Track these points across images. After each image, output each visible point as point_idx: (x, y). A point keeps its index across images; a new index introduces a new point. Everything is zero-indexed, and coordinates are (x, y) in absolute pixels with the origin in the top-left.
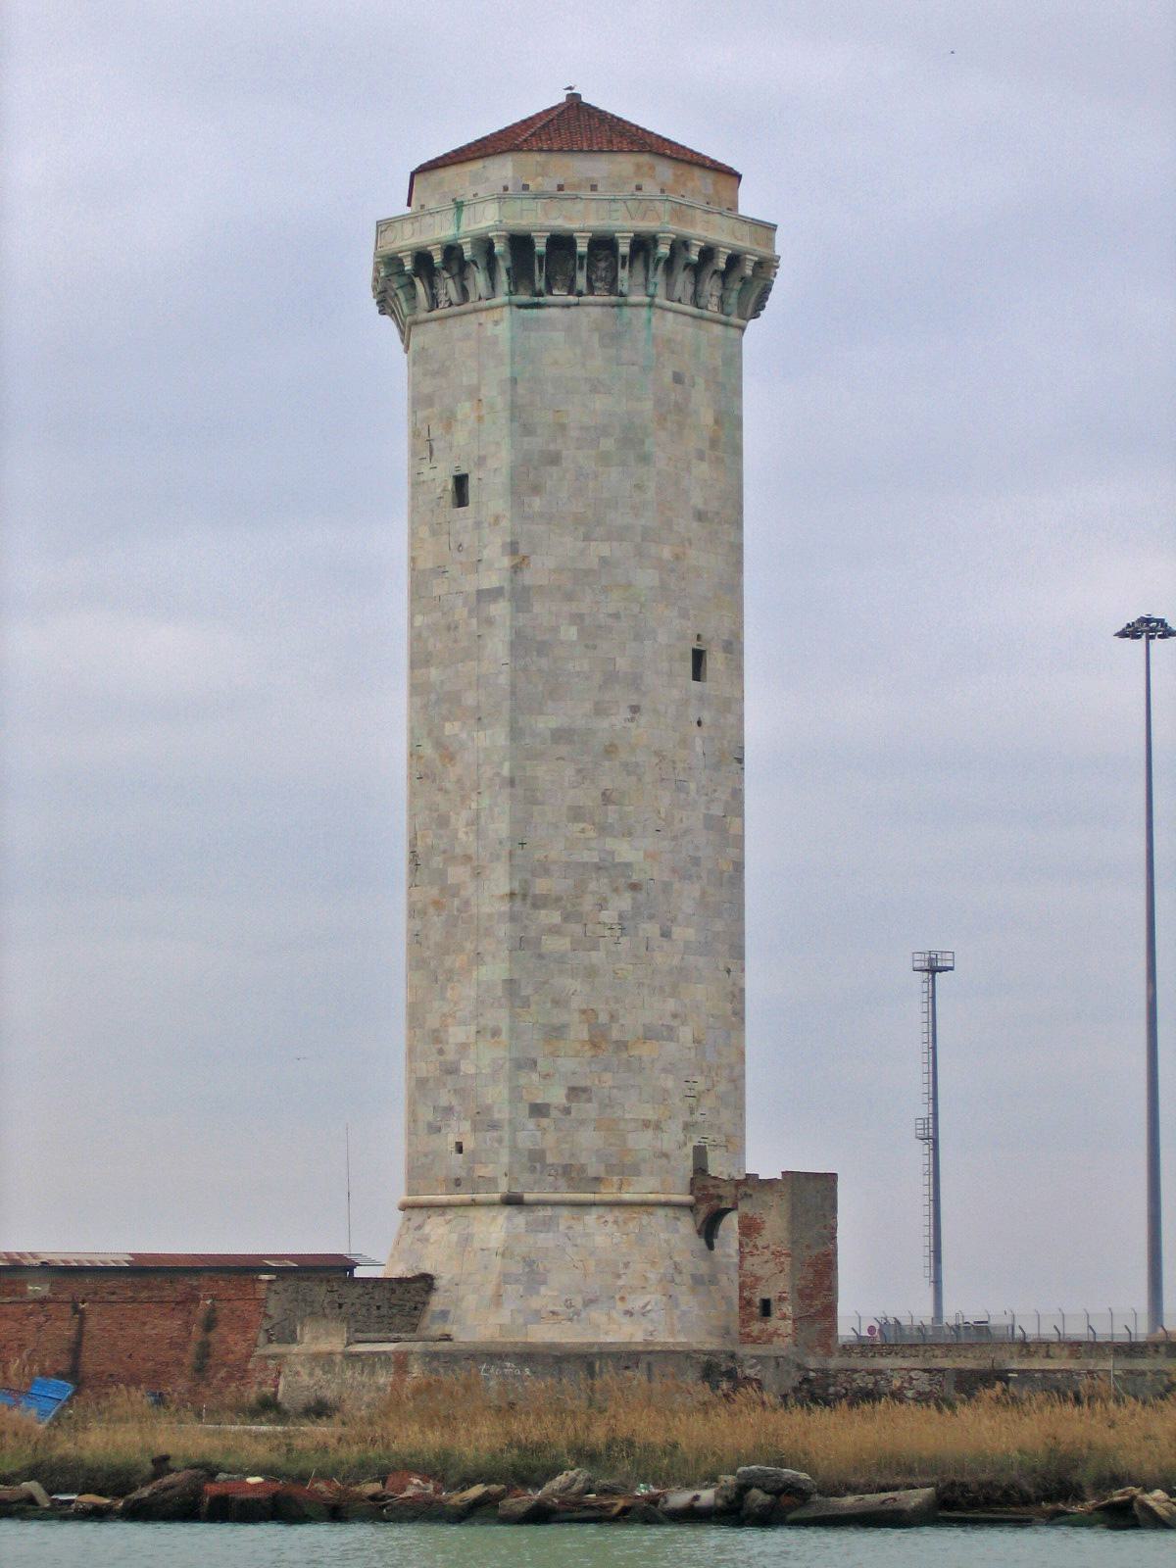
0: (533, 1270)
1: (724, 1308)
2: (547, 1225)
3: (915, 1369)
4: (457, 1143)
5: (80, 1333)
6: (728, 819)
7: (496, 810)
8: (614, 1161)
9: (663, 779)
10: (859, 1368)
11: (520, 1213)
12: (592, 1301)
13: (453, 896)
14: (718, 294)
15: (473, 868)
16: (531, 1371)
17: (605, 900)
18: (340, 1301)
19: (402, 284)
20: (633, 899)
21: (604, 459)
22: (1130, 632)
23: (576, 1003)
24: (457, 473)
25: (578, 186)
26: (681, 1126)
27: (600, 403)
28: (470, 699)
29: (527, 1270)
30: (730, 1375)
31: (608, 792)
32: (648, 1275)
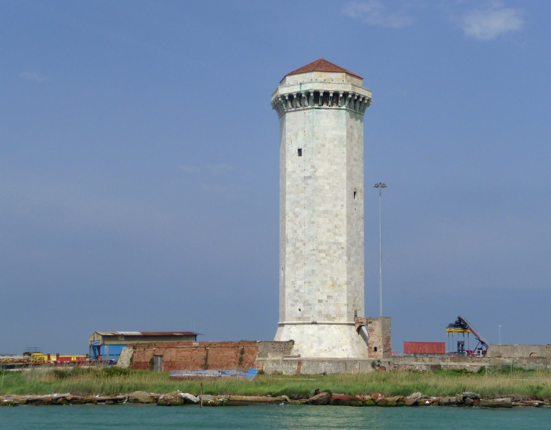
2: (323, 329)
14: (359, 107)
16: (332, 365)
17: (336, 251)
20: (342, 251)
23: (329, 276)
24: (299, 148)
28: (302, 202)
30: (379, 366)
32: (347, 341)
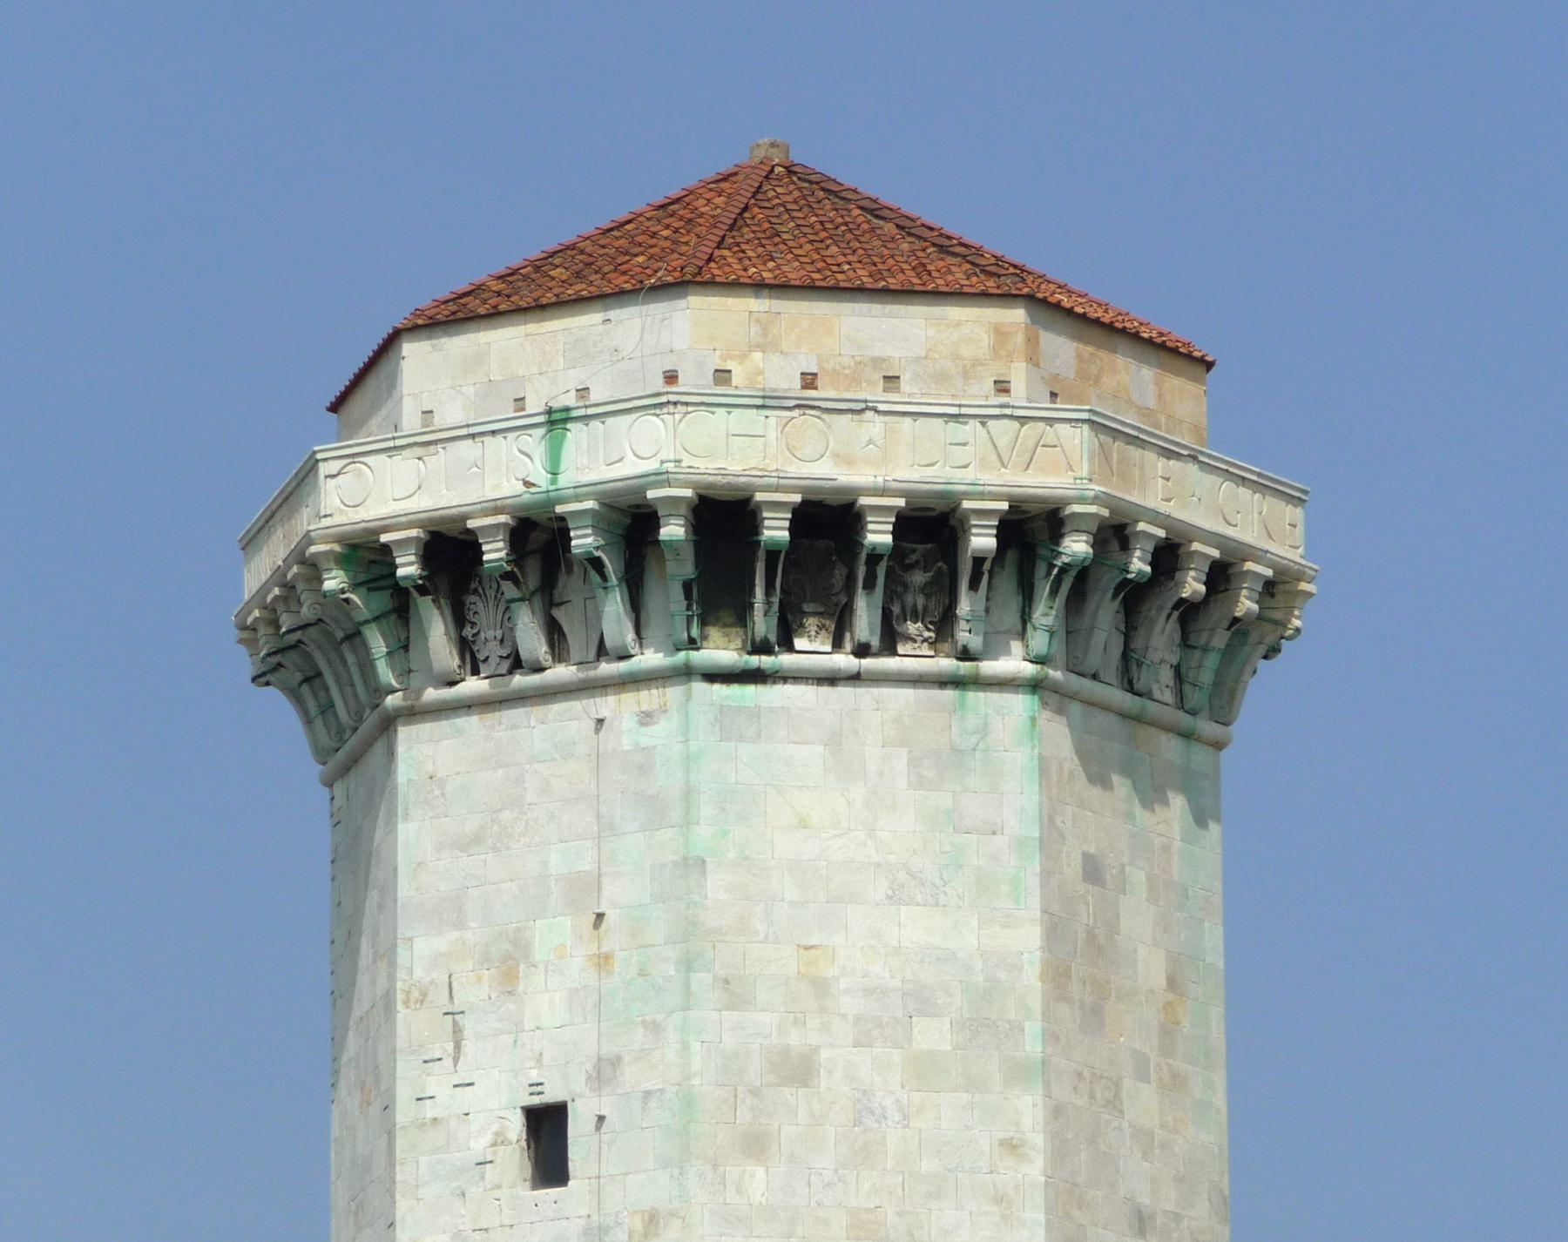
21: (924, 1071)
24: (536, 1101)
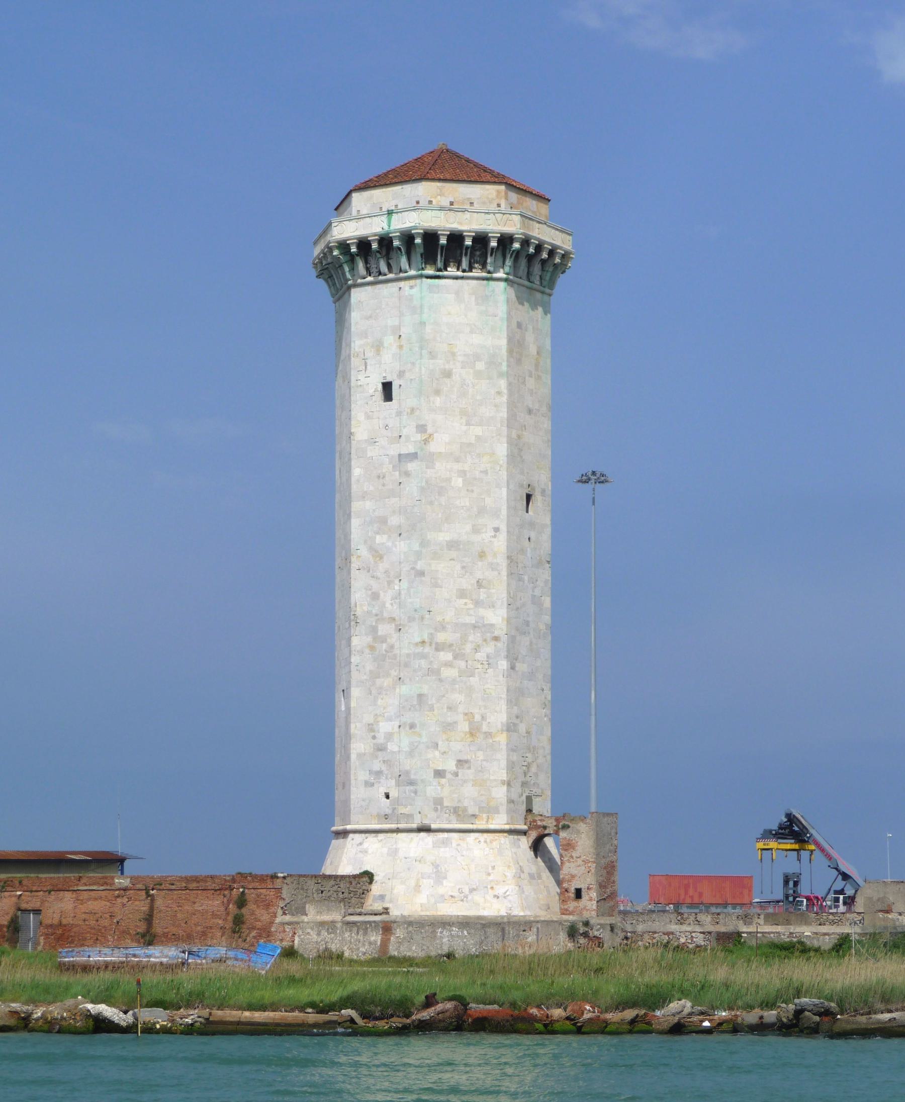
0: (438, 871)
1: (546, 893)
2: (445, 843)
3: (695, 932)
4: (385, 793)
5: (152, 908)
6: (543, 598)
7: (412, 590)
8: (484, 805)
9: (512, 573)
10: (658, 931)
11: (429, 836)
12: (474, 890)
13: (382, 642)
14: (540, 274)
15: (396, 626)
18: (322, 889)
19: (502, 263)
22: (585, 480)
23: (461, 709)
24: (385, 381)
25: (463, 203)
26: (520, 784)
27: (477, 339)
29: (435, 871)
31: (480, 581)
32: (506, 874)
